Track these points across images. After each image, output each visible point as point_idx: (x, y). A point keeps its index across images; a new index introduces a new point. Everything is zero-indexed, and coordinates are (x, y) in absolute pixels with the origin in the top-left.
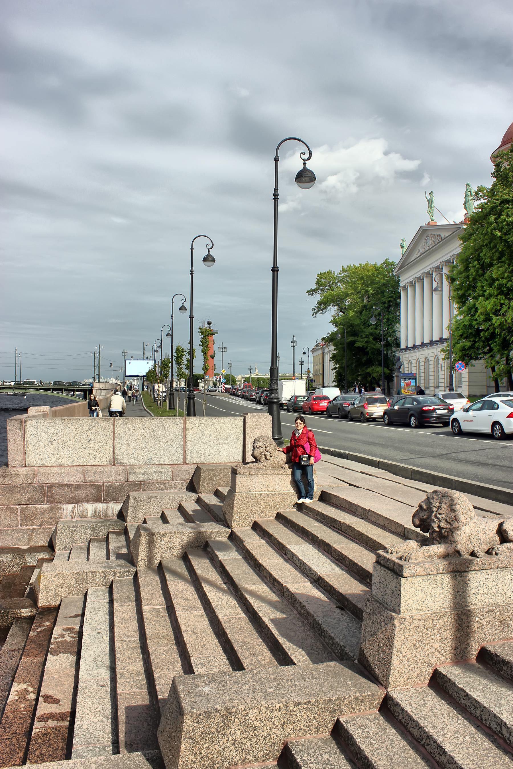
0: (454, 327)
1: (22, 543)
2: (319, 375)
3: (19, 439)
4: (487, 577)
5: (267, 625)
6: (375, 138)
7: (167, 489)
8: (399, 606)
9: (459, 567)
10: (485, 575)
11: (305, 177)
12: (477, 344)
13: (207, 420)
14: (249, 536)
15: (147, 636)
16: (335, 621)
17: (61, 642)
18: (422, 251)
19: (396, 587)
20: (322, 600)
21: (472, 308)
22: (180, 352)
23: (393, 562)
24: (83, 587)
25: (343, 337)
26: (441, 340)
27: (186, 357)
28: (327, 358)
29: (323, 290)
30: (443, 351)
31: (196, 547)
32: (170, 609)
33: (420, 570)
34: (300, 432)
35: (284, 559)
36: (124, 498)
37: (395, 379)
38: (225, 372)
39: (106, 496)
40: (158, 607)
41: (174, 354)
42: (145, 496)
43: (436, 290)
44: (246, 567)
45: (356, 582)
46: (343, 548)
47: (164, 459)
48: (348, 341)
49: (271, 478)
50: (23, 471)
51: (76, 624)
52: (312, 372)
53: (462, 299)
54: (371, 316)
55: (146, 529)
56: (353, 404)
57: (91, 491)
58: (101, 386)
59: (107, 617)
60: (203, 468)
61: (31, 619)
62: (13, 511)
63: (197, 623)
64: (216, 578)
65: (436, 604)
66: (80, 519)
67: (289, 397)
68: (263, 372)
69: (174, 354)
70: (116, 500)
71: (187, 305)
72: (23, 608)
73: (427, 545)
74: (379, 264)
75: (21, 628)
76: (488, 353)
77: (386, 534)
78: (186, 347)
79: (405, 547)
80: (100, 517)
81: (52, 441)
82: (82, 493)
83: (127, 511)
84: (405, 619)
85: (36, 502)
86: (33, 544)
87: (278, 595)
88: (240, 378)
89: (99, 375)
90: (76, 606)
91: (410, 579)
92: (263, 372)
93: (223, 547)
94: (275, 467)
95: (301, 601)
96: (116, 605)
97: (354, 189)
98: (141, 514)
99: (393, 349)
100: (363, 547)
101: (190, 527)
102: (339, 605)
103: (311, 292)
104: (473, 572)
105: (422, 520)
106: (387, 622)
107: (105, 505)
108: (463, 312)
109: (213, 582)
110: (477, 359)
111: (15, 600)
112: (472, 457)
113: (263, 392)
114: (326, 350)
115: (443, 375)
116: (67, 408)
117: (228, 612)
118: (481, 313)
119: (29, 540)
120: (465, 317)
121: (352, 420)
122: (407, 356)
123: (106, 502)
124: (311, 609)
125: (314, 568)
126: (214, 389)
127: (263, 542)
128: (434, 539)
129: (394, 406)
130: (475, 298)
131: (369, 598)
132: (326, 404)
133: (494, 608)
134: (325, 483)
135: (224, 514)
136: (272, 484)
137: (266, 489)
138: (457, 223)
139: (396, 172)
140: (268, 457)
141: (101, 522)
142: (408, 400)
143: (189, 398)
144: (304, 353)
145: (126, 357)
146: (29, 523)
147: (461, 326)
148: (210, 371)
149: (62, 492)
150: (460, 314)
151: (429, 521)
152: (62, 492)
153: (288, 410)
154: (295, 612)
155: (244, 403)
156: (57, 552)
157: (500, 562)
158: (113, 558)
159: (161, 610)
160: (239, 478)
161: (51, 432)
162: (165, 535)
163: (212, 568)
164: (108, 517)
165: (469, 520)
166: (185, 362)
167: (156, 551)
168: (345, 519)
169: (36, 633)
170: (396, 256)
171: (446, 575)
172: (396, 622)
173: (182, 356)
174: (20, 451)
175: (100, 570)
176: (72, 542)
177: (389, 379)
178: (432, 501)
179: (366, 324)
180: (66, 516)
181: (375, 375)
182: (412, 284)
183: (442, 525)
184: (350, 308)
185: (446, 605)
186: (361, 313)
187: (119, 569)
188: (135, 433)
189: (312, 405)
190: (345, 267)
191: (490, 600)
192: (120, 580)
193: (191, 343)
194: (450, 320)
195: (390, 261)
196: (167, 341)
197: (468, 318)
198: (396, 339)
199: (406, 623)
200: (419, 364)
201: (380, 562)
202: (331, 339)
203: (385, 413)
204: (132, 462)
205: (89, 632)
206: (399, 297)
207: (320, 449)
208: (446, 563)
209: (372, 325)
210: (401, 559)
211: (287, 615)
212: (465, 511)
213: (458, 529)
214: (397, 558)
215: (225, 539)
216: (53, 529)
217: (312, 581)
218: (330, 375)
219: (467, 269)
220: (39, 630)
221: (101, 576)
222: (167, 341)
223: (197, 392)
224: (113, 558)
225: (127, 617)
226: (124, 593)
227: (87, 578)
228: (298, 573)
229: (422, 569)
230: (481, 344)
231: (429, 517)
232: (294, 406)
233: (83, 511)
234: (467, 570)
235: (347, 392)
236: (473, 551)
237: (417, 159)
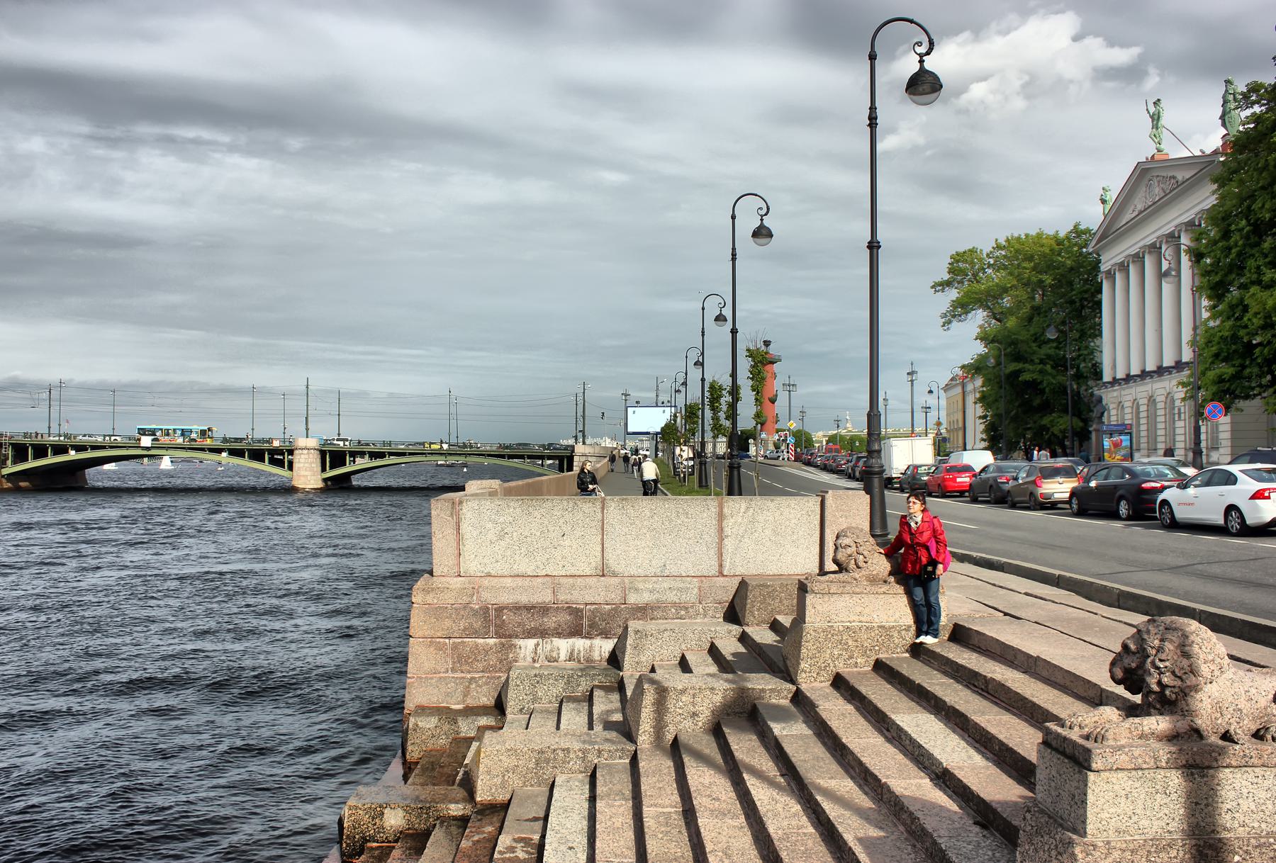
0: (1201, 340)
1: (453, 700)
2: (957, 430)
3: (450, 531)
5: (850, 848)
6: (1057, 13)
7: (690, 617)
8: (1084, 822)
9: (1198, 757)
10: (1251, 777)
11: (923, 85)
12: (1248, 370)
13: (758, 501)
14: (826, 697)
15: (649, 857)
16: (970, 847)
17: (509, 859)
18: (1140, 207)
19: (1078, 788)
20: (949, 811)
21: (1237, 306)
22: (715, 391)
23: (1074, 744)
24: (548, 773)
25: (998, 364)
26: (1179, 366)
27: (726, 399)
28: (970, 399)
29: (961, 282)
30: (1183, 384)
31: (735, 713)
32: (689, 814)
33: (1122, 759)
34: (919, 519)
35: (886, 737)
36: (620, 631)
37: (1093, 436)
38: (793, 425)
39: (590, 626)
40: (669, 810)
41: (707, 394)
42: (653, 627)
43: (1166, 274)
44: (819, 750)
45: (1010, 781)
46: (988, 721)
47: (686, 567)
48: (1008, 371)
49: (866, 599)
50: (456, 583)
51: (534, 832)
52: (944, 425)
53: (1217, 290)
54: (1049, 326)
55: (653, 682)
56: (1016, 479)
58: (587, 450)
59: (585, 823)
60: (752, 583)
61: (463, 821)
62: (440, 648)
63: (732, 840)
64: (766, 764)
65: (1156, 823)
67: (903, 468)
68: (855, 426)
69: (707, 394)
70: (605, 635)
71: (727, 312)
72: (451, 802)
73: (1137, 716)
74: (1062, 234)
75: (448, 833)
76: (1271, 386)
77: (1067, 699)
78: (726, 381)
79: (1096, 718)
80: (579, 661)
81: (502, 535)
82: (550, 622)
83: (624, 653)
84: (1095, 846)
85: (476, 634)
86: (471, 702)
87: (872, 799)
88: (820, 437)
89: (583, 431)
90: (535, 803)
91: (1104, 775)
92: (855, 426)
93: (781, 714)
94: (873, 580)
95: (911, 808)
96: (600, 805)
97: (1019, 103)
98: (646, 659)
99: (1090, 383)
100: (1026, 721)
101: (727, 681)
102: (979, 819)
103: (943, 285)
104: (1227, 770)
105: (1127, 671)
106: (1062, 850)
107: (587, 642)
108: (1221, 314)
109: (763, 771)
110: (1247, 397)
111: (441, 790)
112: (1236, 572)
113: (859, 458)
114: (970, 387)
115: (1182, 429)
116: (528, 485)
117: (786, 823)
118: (1256, 314)
119: (465, 696)
120: (1223, 322)
121: (1014, 506)
122: (1115, 394)
123: (589, 636)
124: (929, 824)
125: (937, 753)
126: (775, 455)
127: (850, 708)
128: (1150, 705)
129: (1089, 481)
130: (1243, 287)
131: (1028, 807)
132: (967, 479)
133: (1272, 840)
134: (961, 611)
135: (785, 659)
136: (867, 610)
137: (856, 618)
138: (1208, 152)
139: (1095, 70)
140: (861, 564)
141: (581, 670)
142: (1113, 471)
143: (731, 467)
144: (931, 392)
145: (628, 401)
147: (1216, 339)
148: (769, 425)
149: (518, 619)
150: (1213, 317)
151: (1140, 672)
152: (518, 619)
153: (902, 490)
154: (901, 828)
155: (825, 477)
156: (509, 717)
158: (598, 728)
159: (674, 816)
160: (810, 599)
161: (502, 519)
162: (683, 691)
163: (762, 750)
165: (1217, 673)
166: (724, 408)
167: (668, 718)
168: (994, 672)
169: (470, 844)
170: (1093, 216)
171: (1174, 772)
172: (1077, 850)
173: (721, 396)
174: (452, 550)
175: (577, 746)
176: (534, 701)
177: (1083, 435)
178: (1146, 637)
179: (1039, 340)
180: (525, 658)
181: (1056, 430)
182: (1124, 267)
183: (1166, 680)
184: (1010, 312)
185: (1174, 826)
186: (1030, 319)
187: (607, 746)
189: (944, 480)
190: (1002, 241)
191: (1264, 826)
192: (607, 765)
193: (734, 375)
194: (1195, 329)
195: (1082, 227)
196: (695, 374)
197: (1230, 323)
198: (1094, 365)
199: (1097, 854)
200: (1138, 408)
201: (1053, 744)
202: (975, 368)
203: (1073, 493)
205: (555, 845)
206: (1100, 291)
207: (955, 555)
208: (1173, 749)
209: (1050, 341)
210: (1087, 737)
211: (887, 832)
212: (1210, 658)
213: (1196, 688)
214: (1081, 736)
215: (785, 702)
216: (503, 679)
217: (933, 776)
218: (976, 428)
219: (1226, 235)
220: (476, 838)
221: (577, 757)
222: (695, 374)
223: (747, 460)
224: (598, 728)
225: (618, 824)
226: (614, 786)
227: (555, 759)
228: (908, 762)
229: (1127, 759)
230: (1256, 370)
231: (1141, 665)
232: (914, 485)
233: (552, 651)
234: (1215, 764)
235: (1005, 458)
236: (1227, 731)
237: (1135, 45)
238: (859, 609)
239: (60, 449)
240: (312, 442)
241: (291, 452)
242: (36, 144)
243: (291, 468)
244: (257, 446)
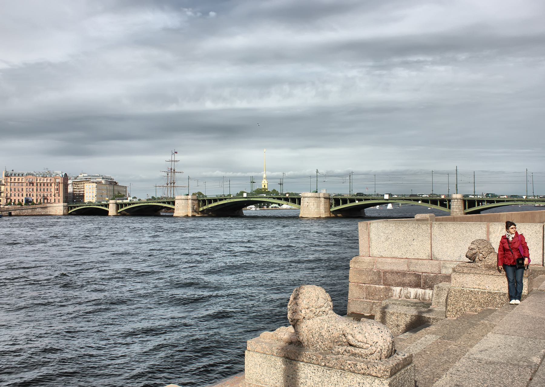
3: (366, 236)
4: (314, 371)
39: (424, 283)
50: (367, 259)
57: (413, 278)
62: (361, 288)
65: (271, 381)
66: (405, 299)
91: (251, 353)
94: (489, 268)
107: (423, 291)
119: (371, 310)
136: (483, 283)
146: (371, 297)
149: (392, 277)
152: (392, 277)
157: (327, 361)
164: (425, 300)
171: (279, 358)
180: (396, 296)
188: (447, 234)
204: (445, 258)
233: (407, 293)
234: (297, 359)
238: (478, 282)
239: (352, 201)
240: (459, 196)
241: (450, 201)
242: (353, 73)
243: (450, 208)
244: (434, 198)
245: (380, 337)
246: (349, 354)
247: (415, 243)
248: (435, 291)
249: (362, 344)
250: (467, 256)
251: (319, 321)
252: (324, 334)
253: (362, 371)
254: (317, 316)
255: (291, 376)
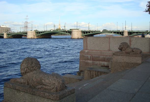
4: (29, 96)
245: (57, 81)
246: (43, 89)
247: (103, 45)
248: (110, 63)
249: (48, 84)
250: (119, 49)
251: (32, 73)
252: (34, 79)
253: (47, 97)
254: (32, 71)
255: (20, 98)
